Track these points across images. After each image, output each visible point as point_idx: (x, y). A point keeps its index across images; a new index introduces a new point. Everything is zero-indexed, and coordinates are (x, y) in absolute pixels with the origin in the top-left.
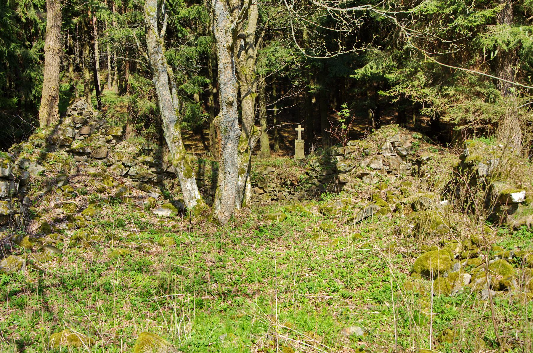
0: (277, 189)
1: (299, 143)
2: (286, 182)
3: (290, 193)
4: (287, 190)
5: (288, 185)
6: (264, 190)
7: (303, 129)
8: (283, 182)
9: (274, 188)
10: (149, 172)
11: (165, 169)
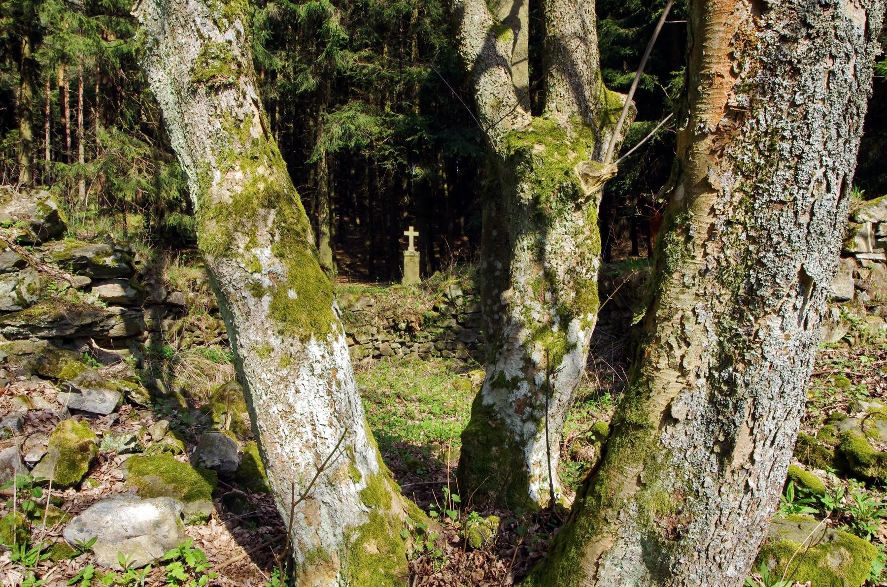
0: (379, 337)
1: (411, 257)
2: (397, 325)
3: (402, 344)
4: (398, 340)
5: (400, 330)
6: (354, 340)
7: (417, 234)
8: (392, 324)
9: (373, 335)
10: (91, 298)
11: (163, 297)
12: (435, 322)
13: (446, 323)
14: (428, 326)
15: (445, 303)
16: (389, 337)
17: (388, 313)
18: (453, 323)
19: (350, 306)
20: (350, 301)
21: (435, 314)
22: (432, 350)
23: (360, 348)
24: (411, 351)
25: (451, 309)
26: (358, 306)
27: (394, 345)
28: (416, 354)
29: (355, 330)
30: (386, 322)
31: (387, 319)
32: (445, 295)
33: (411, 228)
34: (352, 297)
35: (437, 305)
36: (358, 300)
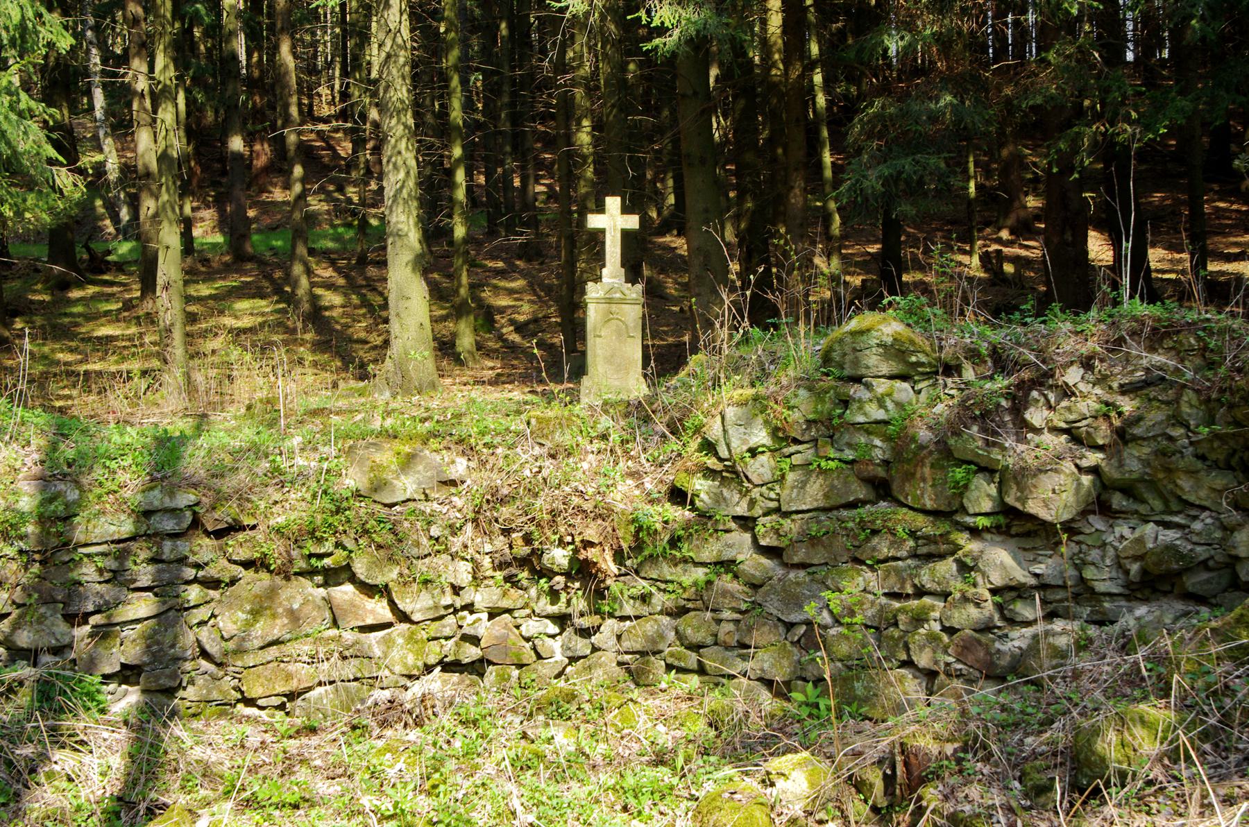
2: (538, 554)
3: (562, 620)
4: (545, 605)
5: (548, 574)
8: (522, 550)
12: (674, 542)
13: (709, 552)
14: (652, 558)
15: (709, 473)
16: (514, 598)
17: (505, 512)
18: (739, 545)
19: (378, 486)
20: (376, 467)
21: (678, 514)
22: (669, 646)
23: (411, 638)
24: (595, 649)
25: (732, 495)
26: (407, 485)
27: (531, 627)
28: (608, 659)
29: (394, 574)
30: (500, 542)
31: (506, 532)
32: (709, 447)
33: (613, 203)
34: (386, 457)
35: (683, 481)
36: (408, 462)
